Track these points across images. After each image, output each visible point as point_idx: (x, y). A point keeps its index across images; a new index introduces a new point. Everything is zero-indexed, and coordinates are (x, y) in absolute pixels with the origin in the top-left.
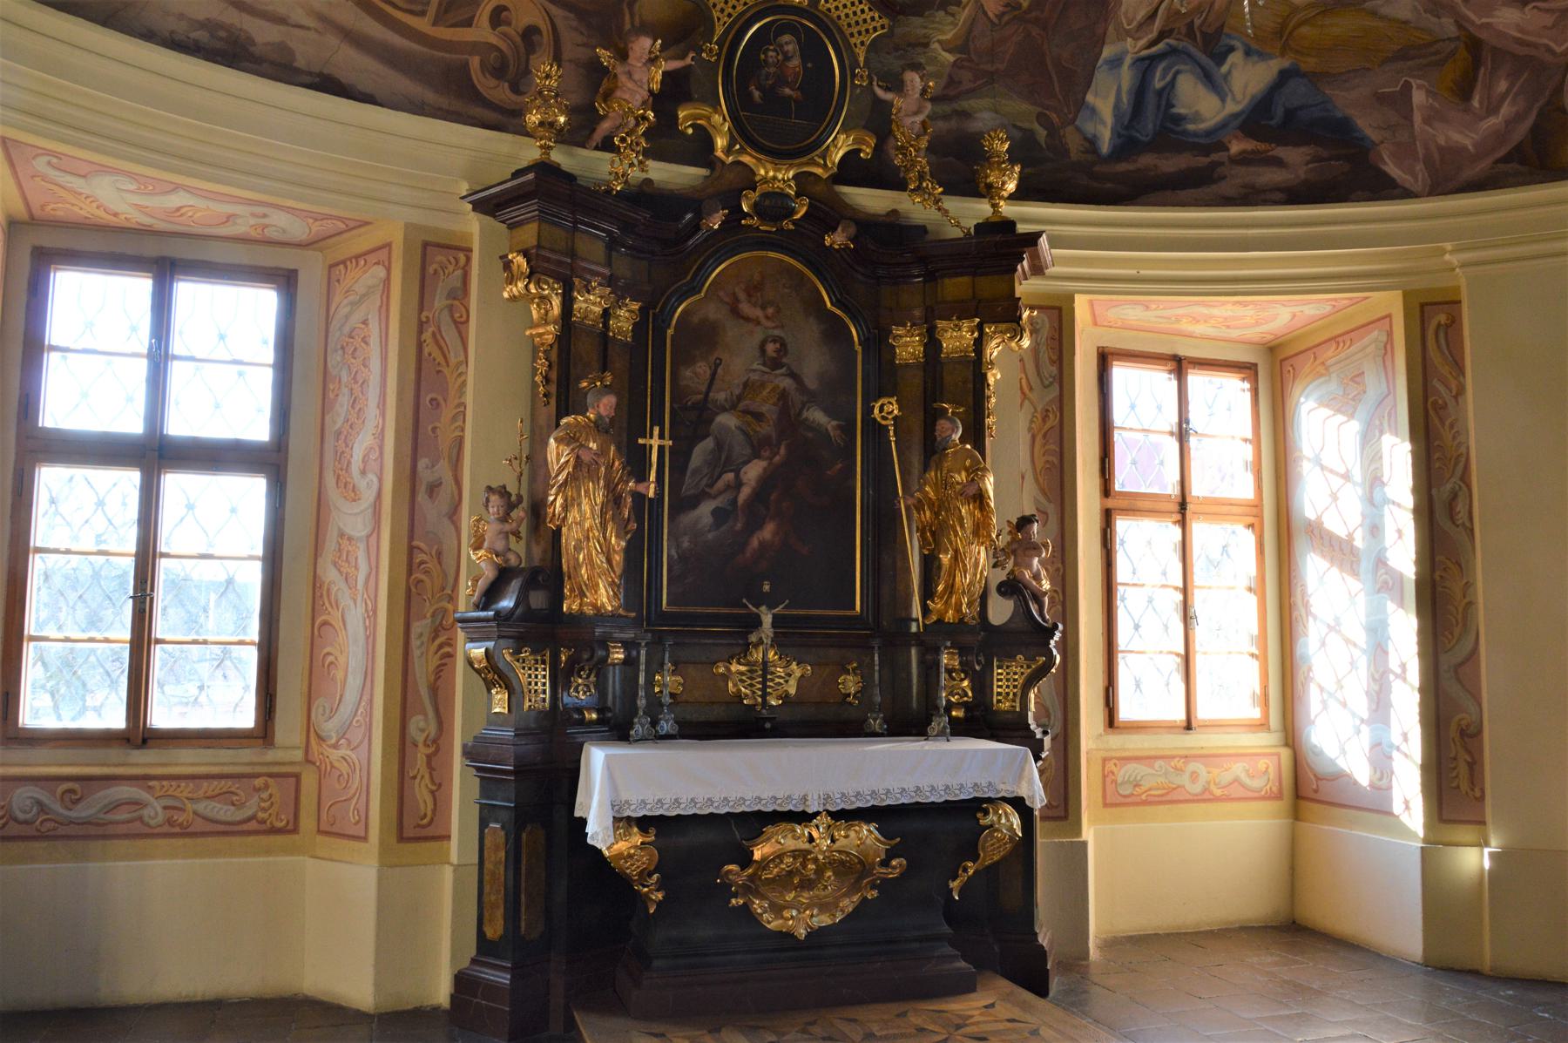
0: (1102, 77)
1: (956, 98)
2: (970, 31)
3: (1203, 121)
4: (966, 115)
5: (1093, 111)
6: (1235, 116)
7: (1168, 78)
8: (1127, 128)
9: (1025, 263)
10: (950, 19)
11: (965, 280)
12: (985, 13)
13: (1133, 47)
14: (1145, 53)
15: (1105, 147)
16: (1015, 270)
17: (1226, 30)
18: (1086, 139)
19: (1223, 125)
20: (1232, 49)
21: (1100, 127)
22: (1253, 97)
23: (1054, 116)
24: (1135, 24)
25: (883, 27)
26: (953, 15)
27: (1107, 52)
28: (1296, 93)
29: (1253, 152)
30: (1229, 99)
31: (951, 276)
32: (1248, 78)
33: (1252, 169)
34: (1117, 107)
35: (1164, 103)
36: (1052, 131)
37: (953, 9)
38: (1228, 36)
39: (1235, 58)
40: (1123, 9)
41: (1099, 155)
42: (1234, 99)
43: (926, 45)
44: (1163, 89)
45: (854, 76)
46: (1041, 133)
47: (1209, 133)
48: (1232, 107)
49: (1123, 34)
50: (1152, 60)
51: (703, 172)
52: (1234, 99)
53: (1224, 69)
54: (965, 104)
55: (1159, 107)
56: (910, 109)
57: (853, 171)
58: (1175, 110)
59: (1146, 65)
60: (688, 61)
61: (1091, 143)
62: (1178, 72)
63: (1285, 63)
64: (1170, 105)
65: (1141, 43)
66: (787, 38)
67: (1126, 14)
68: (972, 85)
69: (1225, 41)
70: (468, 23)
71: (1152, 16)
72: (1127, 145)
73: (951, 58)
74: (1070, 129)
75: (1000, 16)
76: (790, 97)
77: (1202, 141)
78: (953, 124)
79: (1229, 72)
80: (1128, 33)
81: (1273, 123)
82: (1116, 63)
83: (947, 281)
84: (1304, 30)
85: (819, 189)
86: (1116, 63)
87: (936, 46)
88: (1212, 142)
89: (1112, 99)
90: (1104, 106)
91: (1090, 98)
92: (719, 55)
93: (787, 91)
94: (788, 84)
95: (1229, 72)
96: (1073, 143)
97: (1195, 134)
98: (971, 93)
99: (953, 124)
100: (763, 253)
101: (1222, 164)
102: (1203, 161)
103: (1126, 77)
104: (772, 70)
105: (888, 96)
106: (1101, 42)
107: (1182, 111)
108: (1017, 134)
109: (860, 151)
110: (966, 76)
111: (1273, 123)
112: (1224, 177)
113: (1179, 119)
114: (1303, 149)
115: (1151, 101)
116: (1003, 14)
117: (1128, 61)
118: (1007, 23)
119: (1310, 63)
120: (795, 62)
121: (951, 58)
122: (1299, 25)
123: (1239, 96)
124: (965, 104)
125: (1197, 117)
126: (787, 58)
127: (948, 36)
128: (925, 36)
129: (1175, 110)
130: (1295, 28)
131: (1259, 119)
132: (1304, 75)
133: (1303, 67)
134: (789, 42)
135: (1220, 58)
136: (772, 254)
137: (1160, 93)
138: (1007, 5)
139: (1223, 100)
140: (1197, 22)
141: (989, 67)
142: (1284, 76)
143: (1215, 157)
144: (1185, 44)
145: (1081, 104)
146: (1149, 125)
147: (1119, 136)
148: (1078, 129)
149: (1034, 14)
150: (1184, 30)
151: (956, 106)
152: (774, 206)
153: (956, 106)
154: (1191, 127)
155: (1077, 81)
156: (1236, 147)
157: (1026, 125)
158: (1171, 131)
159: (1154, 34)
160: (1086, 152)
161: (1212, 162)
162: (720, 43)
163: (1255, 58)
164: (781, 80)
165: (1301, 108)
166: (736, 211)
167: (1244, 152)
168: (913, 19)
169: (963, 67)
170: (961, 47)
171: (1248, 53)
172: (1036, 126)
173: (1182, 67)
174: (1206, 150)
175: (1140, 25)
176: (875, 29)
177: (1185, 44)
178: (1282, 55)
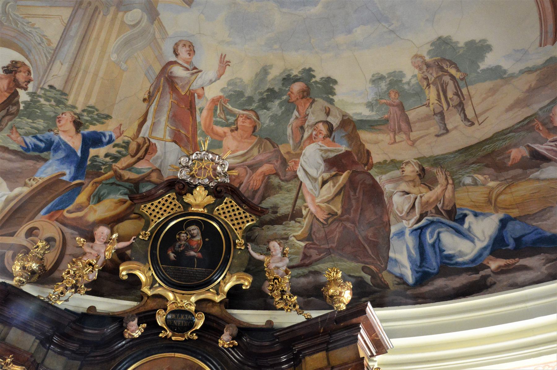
0: (394, 243)
1: (310, 264)
2: (311, 229)
3: (466, 255)
4: (317, 273)
5: (396, 261)
6: (485, 248)
7: (435, 236)
8: (420, 267)
9: (362, 331)
10: (298, 224)
11: (321, 355)
12: (318, 219)
13: (409, 224)
14: (416, 226)
15: (410, 278)
16: (357, 339)
17: (457, 206)
18: (396, 277)
19: (480, 255)
20: (465, 215)
21: (403, 269)
22: (490, 237)
23: (372, 267)
24: (404, 213)
25: (252, 220)
26: (299, 222)
27: (394, 229)
28: (515, 230)
29: (505, 266)
30: (476, 240)
31: (310, 354)
32: (484, 228)
33: (510, 275)
34: (410, 257)
35: (438, 250)
36: (374, 276)
37: (299, 219)
38: (461, 209)
39: (470, 219)
40: (395, 207)
41: (408, 285)
42: (479, 240)
43: (287, 239)
44: (434, 243)
45: (235, 244)
46: (368, 278)
47: (473, 261)
48: (480, 245)
49: (399, 219)
50: (422, 229)
51: (134, 304)
52: (479, 240)
53: (466, 226)
54: (316, 267)
55: (435, 252)
56: (277, 261)
57: (236, 298)
58: (445, 253)
59: (419, 232)
60: (132, 241)
61: (401, 280)
62: (439, 233)
63: (501, 215)
64: (442, 251)
65: (413, 221)
66: (193, 227)
67: (397, 208)
68: (319, 257)
69: (459, 212)
70: (12, 235)
71: (413, 207)
72: (423, 277)
73: (303, 244)
74: (384, 273)
75: (326, 220)
76: (194, 257)
77: (470, 266)
78: (311, 279)
79: (470, 227)
80: (402, 218)
81: (510, 247)
82: (401, 234)
83: (308, 358)
84: (502, 197)
85: (215, 310)
86: (401, 234)
87: (293, 238)
88: (476, 265)
89: (405, 254)
90: (402, 258)
91: (391, 254)
92: (150, 237)
93: (192, 253)
94: (193, 249)
95: (470, 227)
96: (388, 279)
97: (464, 263)
98: (318, 261)
99: (311, 279)
100: (172, 354)
101: (489, 276)
102: (476, 277)
103: (410, 241)
104: (183, 242)
105: (261, 257)
106: (389, 224)
107: (451, 252)
108: (354, 280)
109: (242, 285)
110: (313, 253)
111: (510, 247)
112: (495, 283)
113: (450, 257)
114: (537, 258)
115: (429, 251)
116: (328, 219)
117: (407, 232)
118: (332, 222)
119: (514, 213)
120: (199, 238)
121: (303, 244)
122: (498, 195)
123: (482, 238)
124: (316, 267)
125: (461, 254)
126: (193, 236)
127: (299, 233)
128: (285, 234)
129: (445, 253)
130: (496, 200)
131: (498, 246)
132: (515, 219)
133: (512, 215)
134: (195, 230)
135: (462, 219)
136: (178, 355)
137: (433, 245)
138: (329, 214)
139: (473, 241)
140: (440, 206)
141: (326, 246)
142: (504, 223)
143: (482, 273)
144: (437, 218)
145: (387, 259)
146: (433, 264)
147: (417, 272)
148: (390, 272)
149: (345, 217)
150: (434, 211)
151: (310, 269)
152: (181, 320)
153: (310, 269)
154: (460, 260)
155: (380, 245)
156: (494, 264)
157: (357, 274)
158: (448, 266)
159: (417, 216)
160: (399, 284)
161: (482, 276)
162: (152, 232)
163: (481, 217)
164: (188, 247)
165: (523, 236)
166: (152, 325)
167: (500, 267)
168: (276, 226)
169: (311, 248)
170: (309, 237)
171: (476, 215)
172: (363, 274)
173: (441, 230)
174: (476, 270)
175: (408, 213)
176: (248, 222)
177: (437, 218)
178: (497, 212)
